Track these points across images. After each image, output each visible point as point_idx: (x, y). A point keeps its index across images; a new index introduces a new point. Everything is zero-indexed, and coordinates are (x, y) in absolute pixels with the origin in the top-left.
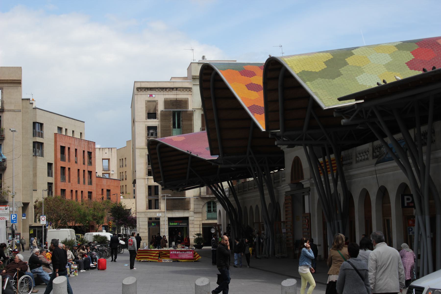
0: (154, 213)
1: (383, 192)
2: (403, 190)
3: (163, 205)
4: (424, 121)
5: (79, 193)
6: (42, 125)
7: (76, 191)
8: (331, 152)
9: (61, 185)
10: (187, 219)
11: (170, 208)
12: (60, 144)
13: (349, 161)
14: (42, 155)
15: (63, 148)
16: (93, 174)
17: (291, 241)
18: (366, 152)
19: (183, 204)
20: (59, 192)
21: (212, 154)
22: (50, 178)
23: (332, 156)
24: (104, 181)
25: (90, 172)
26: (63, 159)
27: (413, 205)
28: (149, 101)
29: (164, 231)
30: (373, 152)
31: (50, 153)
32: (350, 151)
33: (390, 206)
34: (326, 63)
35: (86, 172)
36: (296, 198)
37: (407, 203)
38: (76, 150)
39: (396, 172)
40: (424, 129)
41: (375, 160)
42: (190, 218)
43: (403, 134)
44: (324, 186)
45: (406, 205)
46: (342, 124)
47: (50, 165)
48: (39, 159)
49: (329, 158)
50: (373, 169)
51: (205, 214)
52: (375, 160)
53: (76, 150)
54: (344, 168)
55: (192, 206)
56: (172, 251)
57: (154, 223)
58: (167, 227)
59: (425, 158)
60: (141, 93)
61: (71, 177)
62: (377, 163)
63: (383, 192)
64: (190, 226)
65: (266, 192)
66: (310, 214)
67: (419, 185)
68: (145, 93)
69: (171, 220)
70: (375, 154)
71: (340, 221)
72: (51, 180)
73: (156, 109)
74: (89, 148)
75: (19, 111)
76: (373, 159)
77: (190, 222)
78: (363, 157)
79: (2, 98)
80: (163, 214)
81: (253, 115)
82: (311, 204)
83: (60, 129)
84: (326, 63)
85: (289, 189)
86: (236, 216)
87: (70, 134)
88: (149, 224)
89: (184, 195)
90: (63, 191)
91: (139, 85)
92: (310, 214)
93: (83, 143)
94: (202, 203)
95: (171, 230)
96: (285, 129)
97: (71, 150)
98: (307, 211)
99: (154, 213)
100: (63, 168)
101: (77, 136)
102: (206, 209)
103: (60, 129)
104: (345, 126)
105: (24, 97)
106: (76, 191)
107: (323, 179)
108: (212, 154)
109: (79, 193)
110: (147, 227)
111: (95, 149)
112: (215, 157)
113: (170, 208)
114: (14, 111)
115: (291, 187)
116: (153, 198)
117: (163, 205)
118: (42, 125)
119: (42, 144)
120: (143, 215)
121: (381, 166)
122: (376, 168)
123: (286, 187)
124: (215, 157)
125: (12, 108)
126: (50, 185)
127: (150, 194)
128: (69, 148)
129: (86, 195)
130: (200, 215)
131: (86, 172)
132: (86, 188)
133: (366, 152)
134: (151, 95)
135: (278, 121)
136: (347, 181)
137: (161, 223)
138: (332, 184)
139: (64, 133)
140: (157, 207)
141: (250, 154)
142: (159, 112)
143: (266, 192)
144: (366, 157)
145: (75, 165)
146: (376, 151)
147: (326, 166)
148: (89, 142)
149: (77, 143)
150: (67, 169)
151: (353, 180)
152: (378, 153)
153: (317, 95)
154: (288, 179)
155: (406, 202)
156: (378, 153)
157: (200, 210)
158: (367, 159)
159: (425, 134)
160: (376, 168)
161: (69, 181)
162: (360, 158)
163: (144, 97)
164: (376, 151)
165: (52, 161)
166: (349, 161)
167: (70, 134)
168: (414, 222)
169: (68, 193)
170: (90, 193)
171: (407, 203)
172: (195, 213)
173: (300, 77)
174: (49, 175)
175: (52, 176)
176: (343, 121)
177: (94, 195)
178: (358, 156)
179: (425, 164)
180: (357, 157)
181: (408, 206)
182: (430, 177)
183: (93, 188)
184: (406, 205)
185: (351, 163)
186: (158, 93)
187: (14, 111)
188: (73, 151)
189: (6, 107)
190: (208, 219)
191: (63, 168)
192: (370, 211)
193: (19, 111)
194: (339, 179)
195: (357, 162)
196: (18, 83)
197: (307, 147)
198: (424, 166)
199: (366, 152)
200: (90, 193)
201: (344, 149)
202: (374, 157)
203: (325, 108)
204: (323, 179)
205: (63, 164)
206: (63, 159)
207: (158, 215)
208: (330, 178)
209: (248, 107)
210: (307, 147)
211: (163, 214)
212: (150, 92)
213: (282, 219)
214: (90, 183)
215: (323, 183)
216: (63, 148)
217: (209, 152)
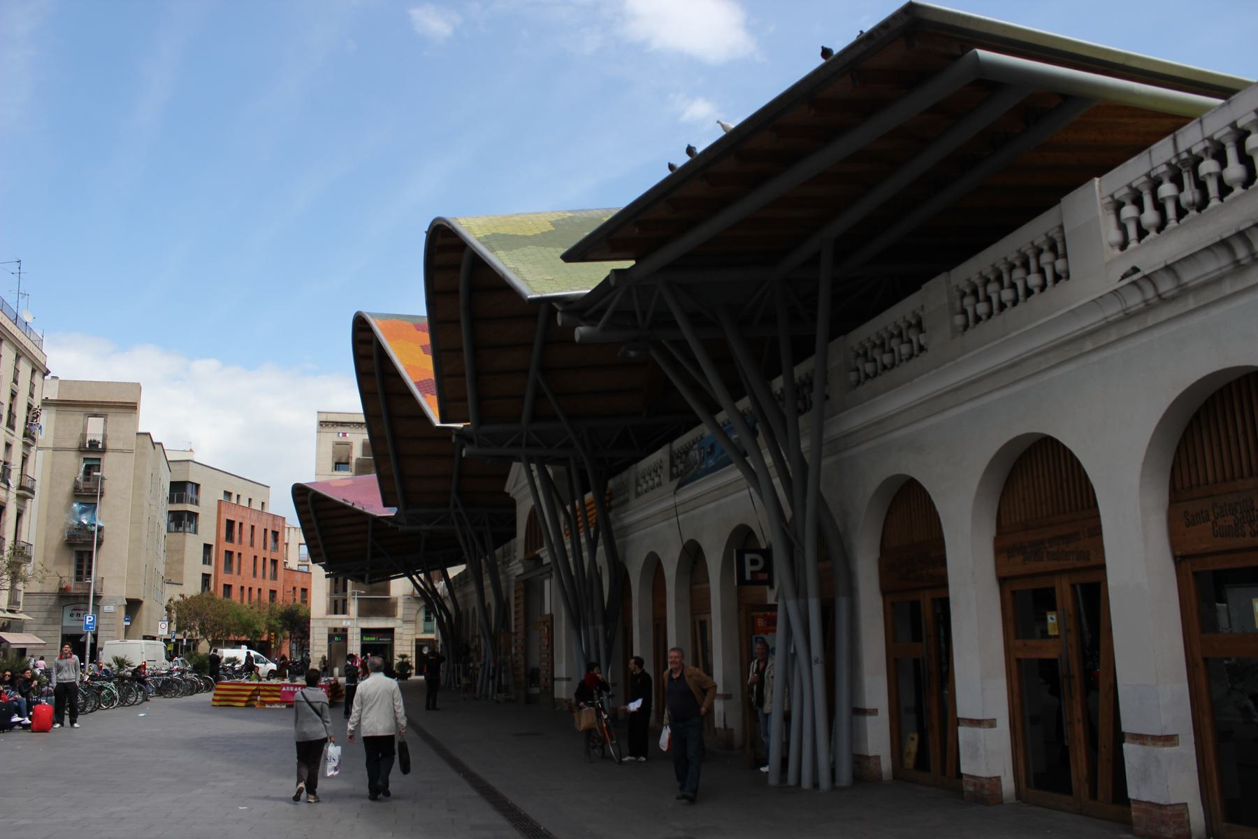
0: (340, 621)
1: (693, 555)
2: (742, 540)
3: (353, 607)
4: (803, 349)
5: (255, 592)
6: (197, 486)
7: (250, 589)
8: (586, 490)
9: (225, 578)
10: (390, 632)
11: (364, 612)
12: (227, 515)
13: (622, 498)
14: (196, 532)
15: (230, 524)
16: (280, 565)
17: (522, 670)
18: (656, 471)
19: (384, 607)
20: (221, 588)
21: (386, 505)
22: (207, 567)
23: (589, 497)
24: (298, 576)
25: (274, 562)
26: (230, 537)
27: (765, 576)
28: (338, 444)
29: (354, 647)
30: (672, 464)
31: (208, 530)
32: (625, 475)
33: (708, 589)
34: (552, 224)
35: (268, 561)
36: (530, 589)
37: (752, 572)
38: (253, 527)
39: (722, 501)
40: (800, 371)
41: (676, 482)
42: (396, 631)
43: (755, 401)
44: (571, 560)
45: (748, 577)
46: (577, 338)
47: (207, 547)
48: (190, 538)
49: (583, 504)
50: (671, 502)
51: (421, 624)
52: (676, 482)
53: (253, 527)
54: (611, 515)
55: (400, 611)
56: (286, 685)
57: (338, 636)
58: (359, 643)
59: (805, 444)
60: (327, 429)
61: (243, 568)
62: (680, 486)
63: (693, 555)
64: (396, 642)
65: (487, 582)
66: (551, 616)
67: (788, 513)
68: (332, 429)
69: (365, 632)
70: (675, 470)
71: (600, 628)
72: (209, 569)
73: (349, 457)
74: (274, 525)
75: (131, 452)
76: (671, 479)
77: (396, 636)
78: (651, 483)
79: (105, 430)
80: (353, 622)
81: (424, 396)
82: (551, 599)
83: (228, 494)
84: (552, 224)
85: (521, 571)
86: (452, 629)
87: (244, 502)
88: (331, 638)
89: (387, 590)
90: (228, 588)
91: (324, 419)
92: (551, 616)
93: (265, 517)
94: (417, 606)
95: (365, 648)
96: (481, 420)
97: (244, 526)
98: (547, 611)
99: (340, 621)
100: (229, 554)
101: (256, 506)
102: (422, 616)
103: (228, 494)
104: (586, 343)
105: (140, 430)
106: (250, 589)
107: (568, 546)
108: (386, 505)
109: (255, 592)
110: (326, 643)
111: (284, 527)
112: (391, 512)
113: (364, 612)
114: (121, 451)
115: (524, 567)
116: (339, 597)
117: (353, 607)
118: (197, 486)
119: (196, 514)
120: (320, 624)
121: (689, 492)
122: (678, 499)
123: (517, 568)
124: (391, 512)
125: (120, 446)
126: (206, 577)
127: (336, 592)
128: (241, 524)
129: (266, 596)
130: (412, 626)
131: (268, 561)
132: (267, 585)
133: (656, 471)
134: (344, 435)
135: (465, 399)
136: (617, 542)
137: (350, 637)
138: (585, 554)
139: (234, 500)
140: (344, 612)
141: (456, 506)
142: (353, 461)
143: (487, 582)
144: (657, 480)
145: (247, 551)
146: (678, 461)
147: (576, 517)
148: (274, 516)
149: (254, 517)
150: (236, 555)
151: (631, 537)
152: (681, 467)
153: (517, 271)
154: (520, 552)
155: (749, 569)
156: (681, 467)
157: (413, 618)
158: (659, 485)
159: (808, 383)
160: (678, 499)
161: (239, 573)
162: (645, 486)
163: (333, 436)
164: (678, 461)
165: (212, 541)
166: (622, 498)
167: (244, 502)
168: (772, 622)
169: (235, 592)
170: (273, 593)
171: (752, 572)
172: (405, 622)
173: (483, 243)
174: (204, 562)
175: (210, 563)
176: (581, 331)
177: (279, 595)
178: (641, 481)
179: (808, 460)
180: (638, 484)
181: (755, 582)
182: (820, 499)
183: (278, 585)
184: (748, 577)
185: (626, 501)
186: (354, 430)
187: (121, 451)
188: (247, 528)
189: (110, 445)
190: (426, 631)
191: (229, 554)
192: (663, 605)
193: (131, 452)
194: (600, 541)
195: (638, 495)
196: (132, 407)
197: (533, 466)
198: (804, 467)
199: (655, 470)
200: (273, 593)
201: (613, 474)
202: (672, 477)
203: (531, 295)
204: (568, 546)
205: (229, 547)
206: (230, 537)
207: (344, 624)
208: (583, 540)
209: (417, 384)
210: (533, 466)
211: (353, 622)
212: (340, 429)
213: (513, 630)
214: (274, 576)
215: (570, 554)
216: (230, 524)
217: (378, 496)
